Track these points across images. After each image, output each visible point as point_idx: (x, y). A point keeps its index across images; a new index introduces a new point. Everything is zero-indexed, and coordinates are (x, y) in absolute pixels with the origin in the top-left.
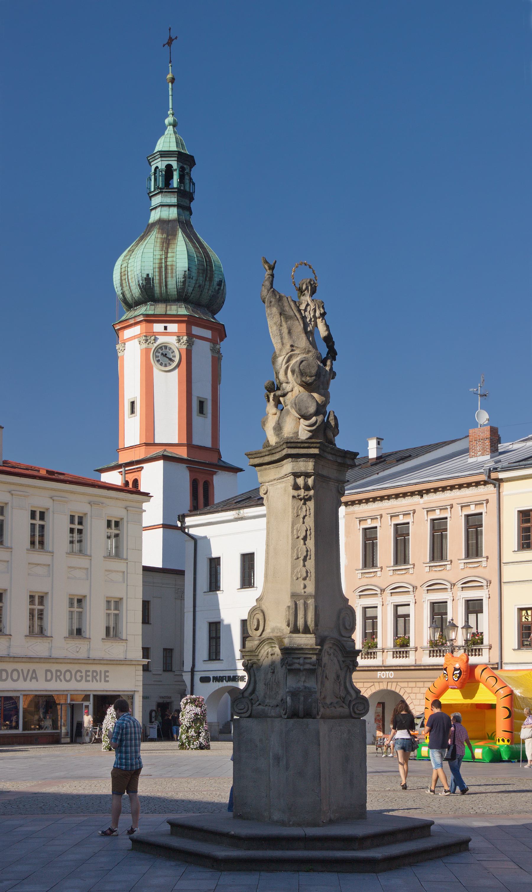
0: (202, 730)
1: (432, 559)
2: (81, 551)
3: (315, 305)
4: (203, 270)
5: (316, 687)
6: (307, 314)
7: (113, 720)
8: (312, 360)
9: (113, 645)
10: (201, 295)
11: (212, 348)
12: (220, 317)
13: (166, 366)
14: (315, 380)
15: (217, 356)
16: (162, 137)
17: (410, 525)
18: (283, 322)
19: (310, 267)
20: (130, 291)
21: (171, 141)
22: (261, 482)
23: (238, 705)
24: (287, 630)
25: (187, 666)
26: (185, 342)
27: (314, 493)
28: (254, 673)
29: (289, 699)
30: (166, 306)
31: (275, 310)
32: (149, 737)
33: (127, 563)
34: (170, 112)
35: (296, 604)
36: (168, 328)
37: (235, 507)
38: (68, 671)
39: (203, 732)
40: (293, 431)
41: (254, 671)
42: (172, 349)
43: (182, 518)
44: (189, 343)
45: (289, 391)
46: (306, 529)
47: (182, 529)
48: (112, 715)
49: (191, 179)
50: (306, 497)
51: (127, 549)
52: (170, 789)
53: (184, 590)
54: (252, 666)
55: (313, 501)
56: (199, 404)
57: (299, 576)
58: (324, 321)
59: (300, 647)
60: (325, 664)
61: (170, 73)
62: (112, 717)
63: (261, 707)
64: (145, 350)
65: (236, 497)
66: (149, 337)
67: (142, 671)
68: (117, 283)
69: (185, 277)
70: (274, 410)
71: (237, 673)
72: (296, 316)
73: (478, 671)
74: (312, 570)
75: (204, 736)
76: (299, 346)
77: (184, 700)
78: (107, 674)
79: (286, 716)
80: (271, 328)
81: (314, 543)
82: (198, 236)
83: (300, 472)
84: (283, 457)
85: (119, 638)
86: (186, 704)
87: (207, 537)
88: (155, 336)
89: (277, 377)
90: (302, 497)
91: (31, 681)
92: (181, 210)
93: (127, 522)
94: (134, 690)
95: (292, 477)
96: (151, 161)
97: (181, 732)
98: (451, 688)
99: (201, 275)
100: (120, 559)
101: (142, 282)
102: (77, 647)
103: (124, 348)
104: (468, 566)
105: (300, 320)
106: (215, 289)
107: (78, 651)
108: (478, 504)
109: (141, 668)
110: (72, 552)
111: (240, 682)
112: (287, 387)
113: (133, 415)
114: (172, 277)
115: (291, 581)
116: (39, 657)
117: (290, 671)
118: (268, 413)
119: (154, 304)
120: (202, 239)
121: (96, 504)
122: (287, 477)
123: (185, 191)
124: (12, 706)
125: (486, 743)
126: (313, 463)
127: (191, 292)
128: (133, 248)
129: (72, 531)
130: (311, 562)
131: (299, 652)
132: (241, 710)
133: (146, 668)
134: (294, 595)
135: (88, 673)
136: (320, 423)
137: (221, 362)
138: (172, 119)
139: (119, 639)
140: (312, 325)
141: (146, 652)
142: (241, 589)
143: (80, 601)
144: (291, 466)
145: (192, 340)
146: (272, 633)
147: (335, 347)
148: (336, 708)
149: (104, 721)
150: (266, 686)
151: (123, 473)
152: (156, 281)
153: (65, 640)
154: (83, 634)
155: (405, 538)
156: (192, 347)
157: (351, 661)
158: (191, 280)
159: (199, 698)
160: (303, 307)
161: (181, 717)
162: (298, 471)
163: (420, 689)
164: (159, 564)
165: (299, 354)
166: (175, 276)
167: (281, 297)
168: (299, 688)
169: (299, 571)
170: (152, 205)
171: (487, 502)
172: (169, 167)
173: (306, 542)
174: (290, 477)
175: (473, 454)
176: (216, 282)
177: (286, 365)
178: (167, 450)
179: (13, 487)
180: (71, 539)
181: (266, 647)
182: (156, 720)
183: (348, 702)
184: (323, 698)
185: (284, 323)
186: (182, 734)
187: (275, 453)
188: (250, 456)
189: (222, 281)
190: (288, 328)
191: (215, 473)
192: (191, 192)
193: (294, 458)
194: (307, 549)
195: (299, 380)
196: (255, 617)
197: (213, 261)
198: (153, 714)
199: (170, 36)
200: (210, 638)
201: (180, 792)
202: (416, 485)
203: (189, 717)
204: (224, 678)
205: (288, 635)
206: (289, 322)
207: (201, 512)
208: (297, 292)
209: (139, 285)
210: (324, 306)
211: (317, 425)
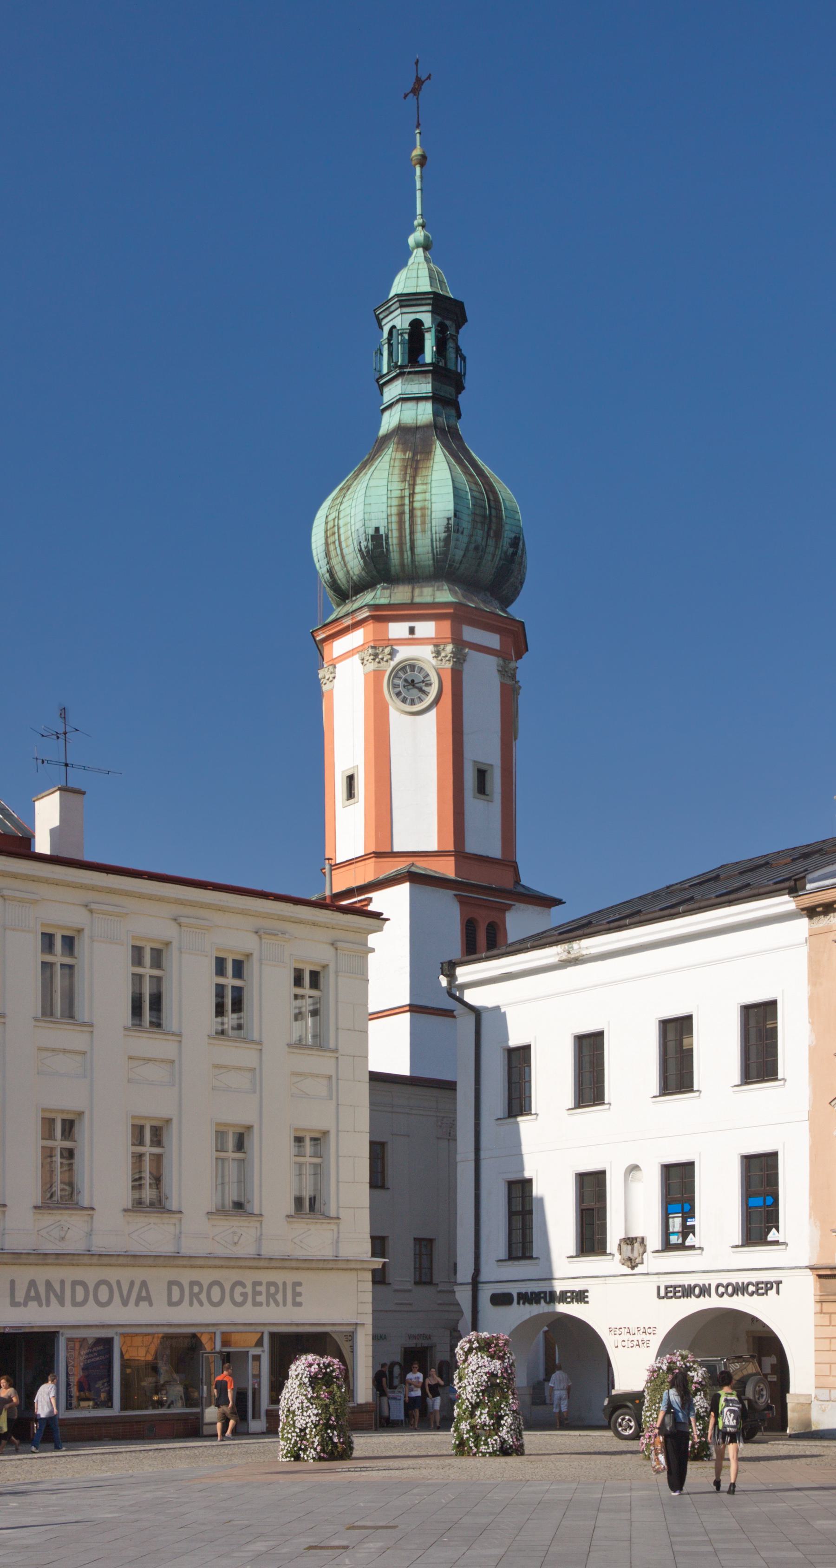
0: (505, 1410)
7: (302, 1390)
9: (309, 1230)
10: (479, 564)
11: (502, 667)
12: (516, 610)
13: (413, 703)
20: (343, 565)
21: (419, 276)
25: (465, 1273)
26: (449, 655)
30: (413, 589)
33: (337, 1058)
34: (419, 220)
36: (417, 631)
38: (215, 1283)
39: (507, 1415)
42: (424, 670)
43: (449, 969)
44: (458, 658)
48: (301, 1379)
49: (458, 350)
51: (337, 1029)
53: (455, 1120)
61: (418, 147)
62: (300, 1384)
64: (373, 673)
66: (381, 649)
67: (371, 1283)
68: (319, 552)
69: (448, 529)
75: (511, 1424)
78: (298, 1289)
91: (137, 1304)
93: (337, 972)
94: (354, 1321)
96: (381, 316)
97: (458, 1415)
99: (479, 525)
101: (365, 543)
102: (234, 1233)
103: (333, 675)
106: (506, 553)
107: (236, 1240)
109: (369, 1276)
111: (557, 1304)
113: (349, 773)
114: (424, 531)
119: (390, 586)
120: (480, 462)
121: (269, 934)
123: (446, 369)
124: (98, 1359)
127: (460, 559)
128: (349, 483)
133: (379, 1278)
135: (258, 1288)
138: (422, 234)
139: (321, 1217)
141: (379, 1245)
142: (575, 1108)
149: (284, 1391)
152: (394, 541)
153: (209, 1219)
154: (248, 1207)
156: (462, 666)
158: (460, 536)
159: (497, 1338)
161: (457, 1381)
163: (830, 1317)
164: (401, 1066)
166: (429, 529)
170: (384, 402)
176: (509, 541)
179: (90, 896)
191: (509, 907)
192: (459, 371)
197: (503, 500)
199: (417, 99)
200: (511, 1214)
203: (475, 1381)
204: (542, 1295)
209: (360, 550)
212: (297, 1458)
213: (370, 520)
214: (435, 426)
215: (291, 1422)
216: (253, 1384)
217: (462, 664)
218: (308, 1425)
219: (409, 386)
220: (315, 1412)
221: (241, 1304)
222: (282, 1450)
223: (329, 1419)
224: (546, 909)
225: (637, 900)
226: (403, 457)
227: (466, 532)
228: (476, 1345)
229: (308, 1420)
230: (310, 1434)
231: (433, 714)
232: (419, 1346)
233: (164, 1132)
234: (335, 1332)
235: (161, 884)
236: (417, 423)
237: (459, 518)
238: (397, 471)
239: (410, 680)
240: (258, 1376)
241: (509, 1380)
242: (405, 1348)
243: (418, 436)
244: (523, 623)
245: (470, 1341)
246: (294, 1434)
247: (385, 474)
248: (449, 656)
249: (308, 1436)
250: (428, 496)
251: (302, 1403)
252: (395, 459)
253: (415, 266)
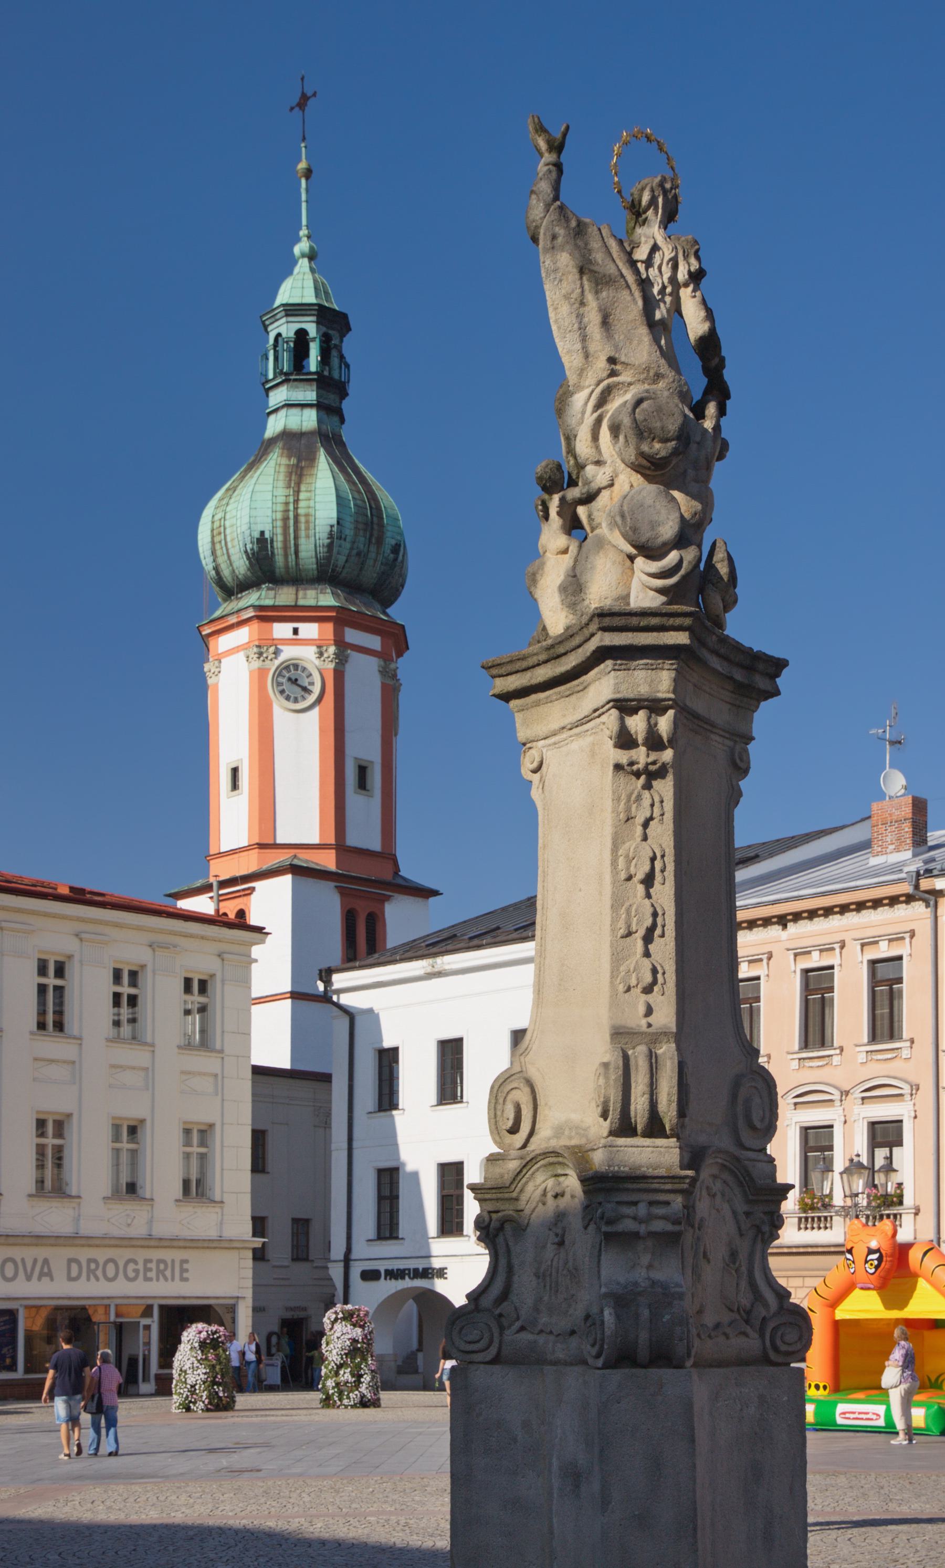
1: (803, 1045)
2: (134, 1038)
3: (676, 248)
4: (366, 524)
5: (683, 1283)
6: (653, 272)
8: (668, 397)
9: (196, 1212)
10: (361, 569)
12: (397, 612)
13: (296, 701)
14: (675, 453)
15: (391, 682)
17: (762, 981)
18: (587, 293)
19: (661, 149)
21: (305, 286)
22: (524, 741)
23: (464, 1332)
24: (599, 1128)
25: (337, 1251)
26: (332, 656)
27: (674, 755)
28: (507, 1245)
29: (610, 1314)
30: (297, 591)
31: (565, 260)
32: (265, 1383)
33: (223, 1058)
34: (303, 232)
35: (626, 1058)
36: (300, 631)
37: (427, 952)
40: (615, 594)
41: (506, 1240)
43: (326, 975)
44: (339, 660)
45: (602, 485)
46: (651, 854)
47: (325, 998)
49: (342, 357)
50: (652, 768)
52: (296, 1509)
53: (330, 1110)
54: (501, 1228)
55: (670, 778)
57: (633, 982)
59: (638, 1173)
60: (702, 1220)
61: (304, 228)
63: (525, 1336)
65: (428, 936)
66: (265, 648)
69: (331, 536)
70: (561, 540)
71: (430, 1263)
72: (622, 276)
73: (914, 1256)
74: (670, 967)
75: (370, 1382)
76: (632, 360)
77: (330, 1315)
78: (185, 1266)
79: (600, 1363)
80: (556, 309)
81: (673, 892)
82: (357, 461)
83: (637, 697)
84: (588, 658)
85: (209, 1199)
86: (333, 1323)
87: (374, 1009)
88: (276, 645)
89: (571, 451)
90: (641, 766)
91: (39, 1279)
92: (323, 413)
93: (223, 981)
95: (614, 713)
96: (267, 323)
97: (326, 1374)
98: (862, 1288)
99: (361, 533)
100: (208, 1051)
102: (128, 1215)
103: (218, 670)
104: (875, 1057)
105: (634, 287)
108: (895, 939)
110: (117, 1039)
112: (596, 476)
113: (236, 792)
114: (308, 537)
115: (611, 997)
116: (56, 1235)
117: (609, 1238)
118: (545, 552)
120: (362, 468)
121: (162, 947)
122: (599, 716)
123: (331, 378)
124: (4, 1328)
125: (931, 1397)
126: (673, 674)
129: (117, 997)
130: (666, 945)
131: (635, 1186)
132: (470, 1343)
133: (259, 1255)
134: (620, 1034)
135: (149, 1265)
136: (691, 567)
137: (398, 695)
139: (206, 1201)
140: (668, 305)
141: (259, 1225)
142: (438, 1105)
143: (133, 1130)
144: (612, 682)
145: (346, 653)
146: (555, 1140)
148: (727, 1337)
149: (177, 1354)
150: (540, 1280)
151: (215, 899)
152: (278, 544)
153: (105, 1203)
154: (140, 1191)
155: (751, 1007)
157: (765, 1213)
158: (342, 542)
159: (359, 1310)
160: (641, 254)
162: (631, 696)
164: (285, 1063)
165: (630, 384)
167: (580, 223)
168: (636, 1284)
169: (632, 969)
171: (912, 936)
172: (301, 335)
173: (651, 890)
174: (607, 714)
175: (879, 849)
177: (596, 415)
178: (300, 856)
180: (116, 1018)
181: (540, 1177)
182: (278, 1350)
183: (757, 1323)
184: (698, 1312)
185: (590, 297)
186: (327, 1377)
187: (565, 654)
188: (495, 671)
189: (400, 545)
191: (388, 898)
192: (343, 380)
193: (621, 659)
194: (655, 909)
195: (631, 454)
196: (510, 1097)
198: (274, 1340)
200: (381, 1198)
201: (318, 1516)
202: (775, 906)
203: (340, 1346)
205: (603, 1141)
206: (604, 294)
207: (363, 963)
208: (627, 215)
209: (246, 552)
210: (700, 253)
211: (682, 572)
212: (188, 1409)
213: (256, 523)
215: (183, 1380)
216: (144, 1351)
217: (344, 665)
218: (198, 1382)
219: (295, 394)
220: (204, 1371)
221: (114, 1279)
222: (175, 1403)
223: (216, 1377)
225: (499, 911)
226: (287, 462)
227: (349, 539)
228: (340, 1315)
229: (198, 1378)
230: (200, 1389)
232: (295, 1317)
233: (66, 1125)
234: (218, 1305)
235: (65, 904)
239: (293, 679)
240: (148, 1344)
241: (368, 1344)
242: (282, 1319)
243: (303, 442)
244: (403, 627)
245: (336, 1313)
246: (186, 1390)
247: (271, 479)
249: (197, 1391)
250: (312, 503)
251: (193, 1363)
252: (280, 465)
253: (301, 276)
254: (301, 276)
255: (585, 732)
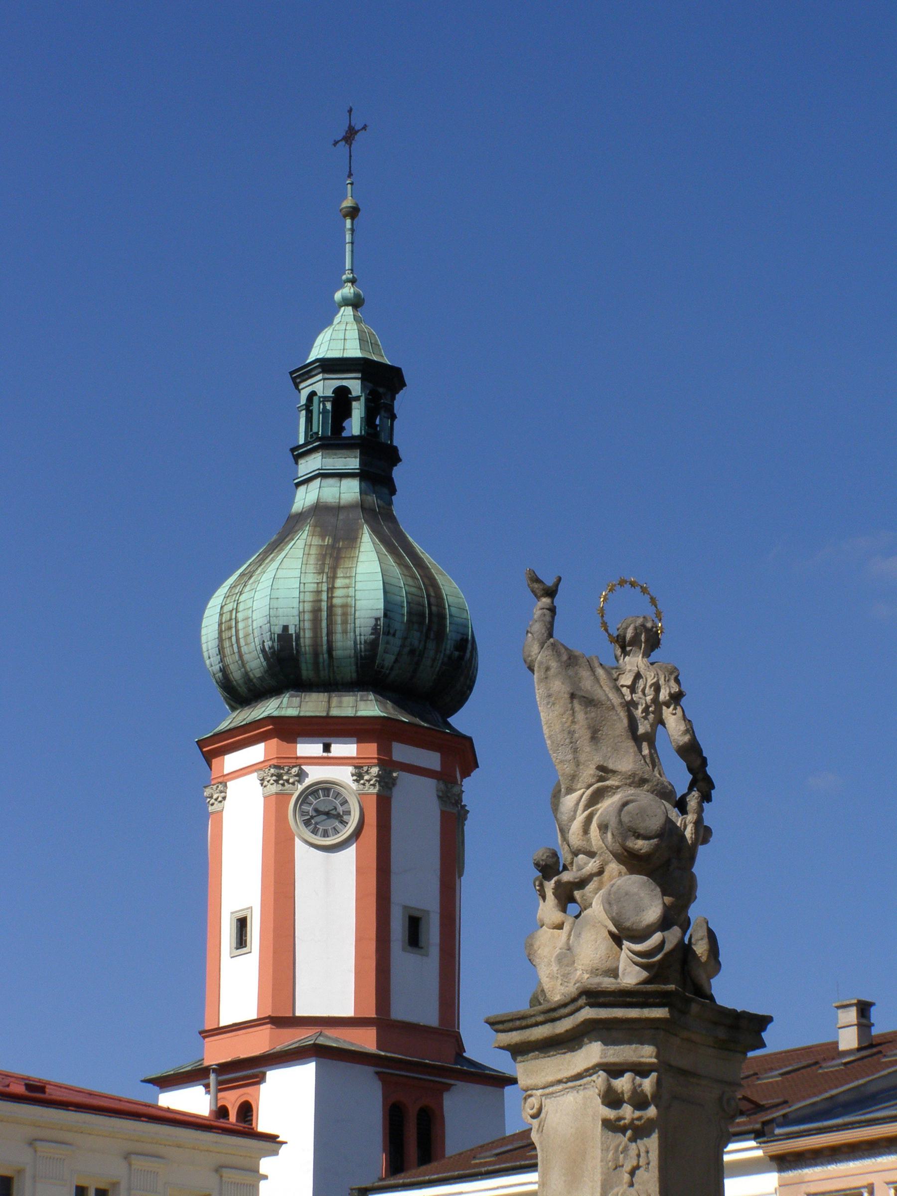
11: (442, 791)
12: (460, 721)
13: (326, 834)
15: (455, 811)
16: (326, 330)
30: (329, 698)
31: (559, 686)
55: (655, 1136)
56: (409, 925)
58: (679, 710)
69: (375, 630)
82: (410, 539)
99: (416, 626)
101: (270, 643)
113: (241, 915)
114: (345, 632)
138: (352, 290)
147: (710, 770)
158: (390, 638)
165: (618, 787)
177: (587, 813)
188: (500, 1027)
190: (589, 728)
191: (448, 1087)
195: (617, 848)
199: (350, 148)
214: (363, 507)
217: (390, 789)
224: (498, 1089)
226: (320, 543)
227: (398, 634)
231: (351, 852)
236: (339, 502)
237: (390, 618)
238: (312, 560)
243: (341, 517)
248: (374, 780)
253: (343, 327)
254: (343, 327)
255: (579, 1086)
